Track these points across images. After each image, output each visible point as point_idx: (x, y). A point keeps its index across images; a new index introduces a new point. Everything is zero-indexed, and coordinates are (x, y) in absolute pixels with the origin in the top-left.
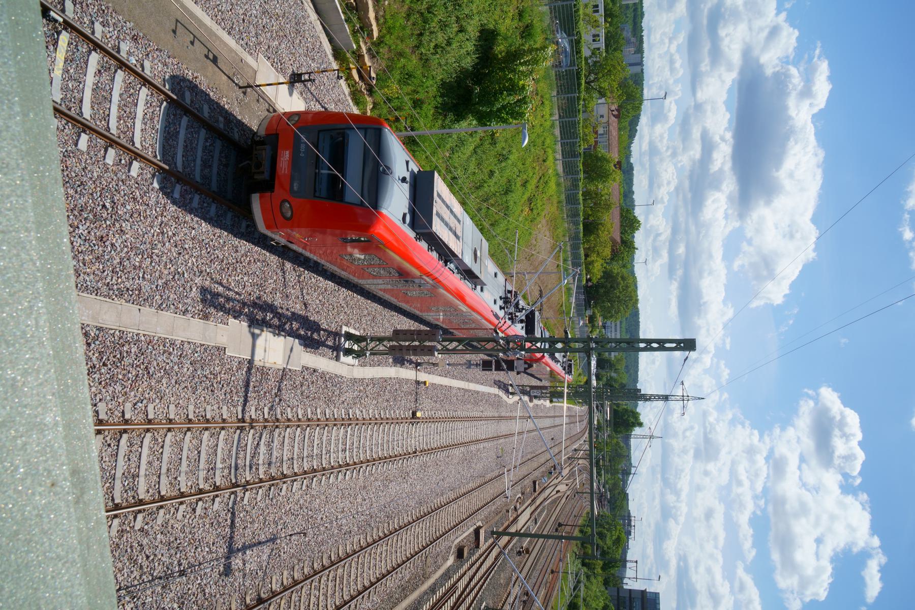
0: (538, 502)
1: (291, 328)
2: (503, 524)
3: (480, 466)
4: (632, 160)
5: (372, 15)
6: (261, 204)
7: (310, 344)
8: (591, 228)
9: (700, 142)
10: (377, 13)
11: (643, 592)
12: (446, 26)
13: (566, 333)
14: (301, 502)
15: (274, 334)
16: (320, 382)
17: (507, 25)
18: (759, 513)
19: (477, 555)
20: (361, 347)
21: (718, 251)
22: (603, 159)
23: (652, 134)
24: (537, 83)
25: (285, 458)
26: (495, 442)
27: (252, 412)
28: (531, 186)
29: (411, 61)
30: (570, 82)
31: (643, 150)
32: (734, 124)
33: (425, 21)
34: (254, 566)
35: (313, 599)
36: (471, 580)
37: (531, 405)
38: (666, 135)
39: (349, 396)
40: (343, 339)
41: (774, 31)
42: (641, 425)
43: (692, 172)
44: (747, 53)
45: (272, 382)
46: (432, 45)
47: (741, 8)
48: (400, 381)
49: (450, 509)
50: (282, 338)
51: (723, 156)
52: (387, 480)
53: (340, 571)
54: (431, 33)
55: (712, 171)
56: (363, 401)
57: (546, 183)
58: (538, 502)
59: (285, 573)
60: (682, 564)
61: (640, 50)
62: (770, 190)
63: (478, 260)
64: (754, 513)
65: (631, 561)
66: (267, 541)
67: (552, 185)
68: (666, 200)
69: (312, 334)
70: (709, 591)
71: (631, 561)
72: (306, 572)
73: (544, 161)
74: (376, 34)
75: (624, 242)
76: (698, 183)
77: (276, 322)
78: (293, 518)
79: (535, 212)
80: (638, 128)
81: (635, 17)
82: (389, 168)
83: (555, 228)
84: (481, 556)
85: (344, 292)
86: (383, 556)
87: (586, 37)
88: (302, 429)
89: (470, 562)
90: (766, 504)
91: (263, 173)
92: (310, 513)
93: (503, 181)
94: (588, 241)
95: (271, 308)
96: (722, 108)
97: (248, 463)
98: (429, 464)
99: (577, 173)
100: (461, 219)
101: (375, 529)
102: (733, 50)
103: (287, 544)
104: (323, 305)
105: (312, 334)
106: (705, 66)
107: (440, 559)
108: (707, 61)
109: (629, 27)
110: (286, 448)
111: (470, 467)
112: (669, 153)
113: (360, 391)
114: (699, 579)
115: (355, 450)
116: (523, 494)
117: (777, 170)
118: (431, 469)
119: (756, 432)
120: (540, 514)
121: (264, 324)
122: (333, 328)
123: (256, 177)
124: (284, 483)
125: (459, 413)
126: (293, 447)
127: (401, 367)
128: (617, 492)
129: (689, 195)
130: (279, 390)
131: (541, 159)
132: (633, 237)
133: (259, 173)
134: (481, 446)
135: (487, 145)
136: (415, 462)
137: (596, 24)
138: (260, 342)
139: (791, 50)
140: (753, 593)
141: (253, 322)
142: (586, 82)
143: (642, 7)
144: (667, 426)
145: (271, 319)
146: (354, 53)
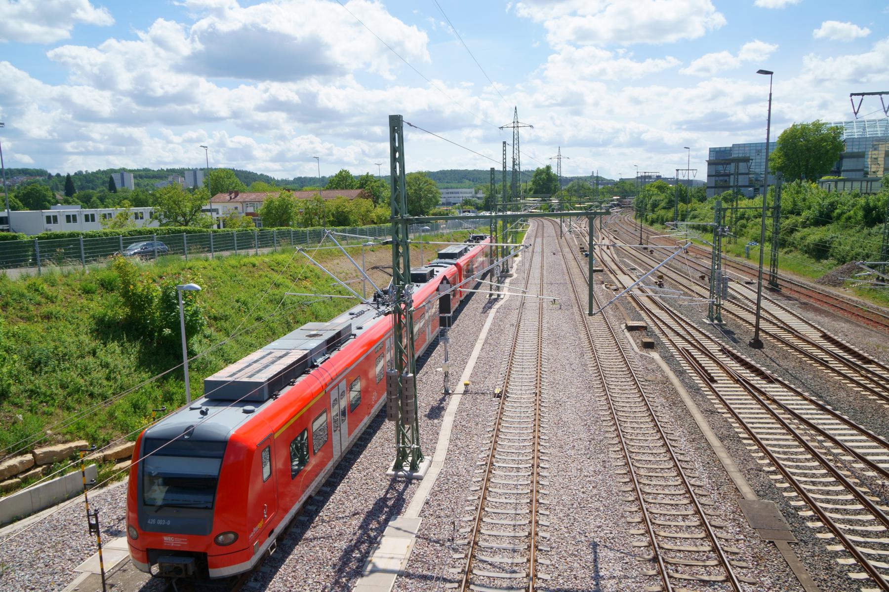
0: (614, 267)
1: (376, 529)
2: (629, 302)
3: (565, 327)
4: (291, 179)
5: (59, 448)
6: (224, 566)
7: (397, 508)
8: (341, 219)
9: (270, 113)
10: (59, 442)
11: (710, 163)
12: (86, 369)
13: (387, 243)
14: (561, 515)
15: (378, 548)
16: (441, 497)
17: (100, 305)
18: (632, 54)
19: (655, 329)
20: (409, 456)
22: (269, 207)
23: (263, 160)
24: (147, 273)
25: (512, 534)
26: (545, 311)
27: (454, 572)
28: (278, 278)
29: (120, 405)
30: (177, 241)
31: (280, 168)
32: (250, 81)
33: (78, 390)
34: (618, 567)
35: (667, 501)
36: (678, 334)
37: (515, 276)
38: (264, 146)
39: (462, 465)
40: (400, 473)
41: (159, 42)
42: (548, 168)
43: (299, 121)
44: (179, 69)
45: (429, 550)
46: (105, 383)
47: (135, 74)
48: (460, 411)
49: (603, 356)
50: (384, 539)
51: (284, 91)
52: (560, 423)
53: (642, 472)
54: (91, 384)
55: (300, 102)
56: (471, 451)
57: (278, 264)
58: (614, 267)
59: (632, 531)
60: (684, 127)
61: (181, 172)
62: (315, 46)
63: (320, 333)
64: (631, 59)
65: (677, 175)
66: (596, 552)
67: (280, 257)
69: (387, 506)
70: (709, 100)
71: (677, 175)
72: (636, 509)
73: (254, 266)
74: (83, 443)
75: (361, 186)
76: (311, 115)
77: (364, 547)
78: (576, 524)
79: (308, 275)
80: (259, 173)
81: (148, 177)
82: (188, 428)
83: (330, 254)
84: (656, 324)
85: (354, 473)
86: (636, 425)
87: (139, 225)
88: (485, 516)
89: (661, 336)
90: (621, 47)
91: (186, 565)
92: (575, 506)
93: (269, 307)
94: (355, 221)
95: (348, 552)
96: (235, 91)
97: (508, 575)
98: (552, 379)
100: (268, 352)
101: (607, 435)
102: (179, 82)
103: (603, 530)
104: (359, 494)
105: (387, 506)
106: (196, 110)
107: (650, 367)
108: (189, 107)
109: (157, 182)
110: (502, 533)
111: (564, 337)
112: (282, 143)
113: (460, 453)
114: (699, 111)
115: (520, 458)
116: (603, 283)
117: (295, 39)
118: (557, 377)
119: (550, 58)
120: (627, 265)
121: (363, 560)
122: (386, 484)
123: (191, 573)
124: (537, 534)
125: (507, 349)
126: (502, 525)
127: (445, 410)
128: (616, 190)
129: (324, 123)
130: (437, 542)
131: (252, 269)
132: (356, 177)
133: (186, 570)
134: (545, 325)
135: (226, 325)
136: (547, 394)
137: (126, 216)
138: (381, 564)
139: (178, 26)
140: (709, 59)
141: (359, 573)
142: (186, 225)
143: (138, 170)
144: (550, 143)
145: (360, 552)
146: (100, 466)
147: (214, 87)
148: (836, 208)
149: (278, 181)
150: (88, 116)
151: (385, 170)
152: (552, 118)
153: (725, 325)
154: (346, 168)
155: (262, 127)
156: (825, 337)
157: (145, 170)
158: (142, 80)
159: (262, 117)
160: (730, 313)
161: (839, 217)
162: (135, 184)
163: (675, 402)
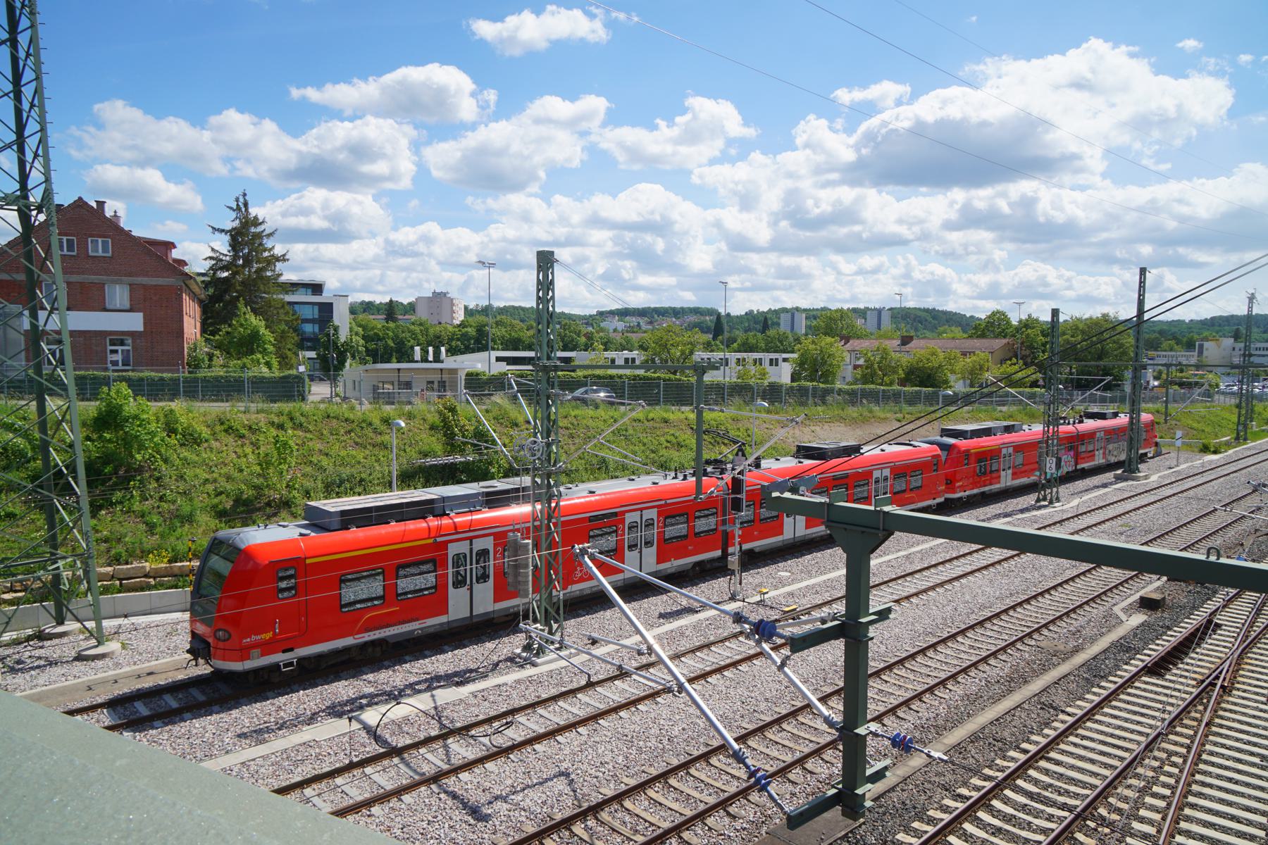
38: (964, 278)
43: (1013, 240)
51: (982, 197)
62: (1031, 125)
68: (1068, 274)
74: (586, 559)
76: (1034, 233)
108: (857, 228)
147: (891, 199)
150: (740, 244)
158: (792, 196)
159: (955, 237)
160: (1103, 522)
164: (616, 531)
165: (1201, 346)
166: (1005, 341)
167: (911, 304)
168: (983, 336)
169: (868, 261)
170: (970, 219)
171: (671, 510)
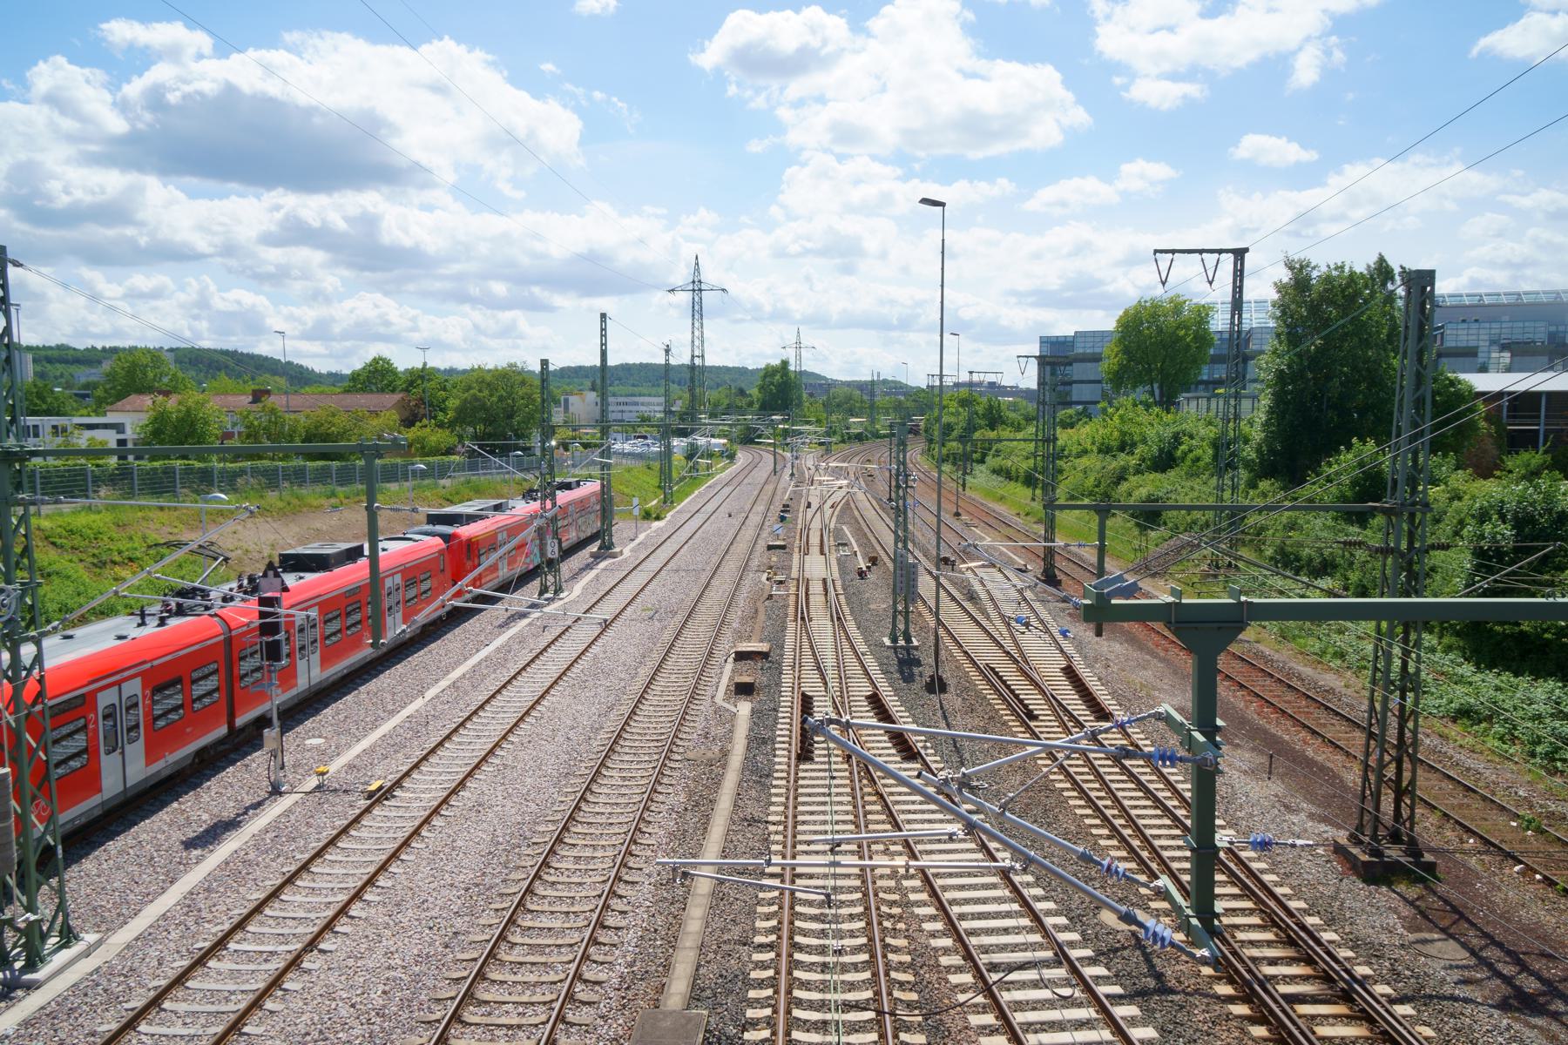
21: (495, 224)
38: (285, 310)
42: (785, 363)
43: (350, 265)
51: (315, 207)
62: (370, 127)
68: (413, 312)
99: (169, 472)
108: (130, 231)
114: (1051, 276)
148: (1181, 444)
149: (321, 375)
151: (596, 361)
152: (808, 279)
153: (916, 648)
154: (386, 354)
155: (276, 278)
156: (1070, 672)
157: (60, 347)
159: (274, 255)
161: (1183, 459)
162: (36, 373)
163: (701, 804)
164: (85, 727)
165: (566, 401)
166: (397, 397)
167: (206, 344)
168: (364, 390)
169: (141, 280)
170: (296, 233)
171: (166, 676)
